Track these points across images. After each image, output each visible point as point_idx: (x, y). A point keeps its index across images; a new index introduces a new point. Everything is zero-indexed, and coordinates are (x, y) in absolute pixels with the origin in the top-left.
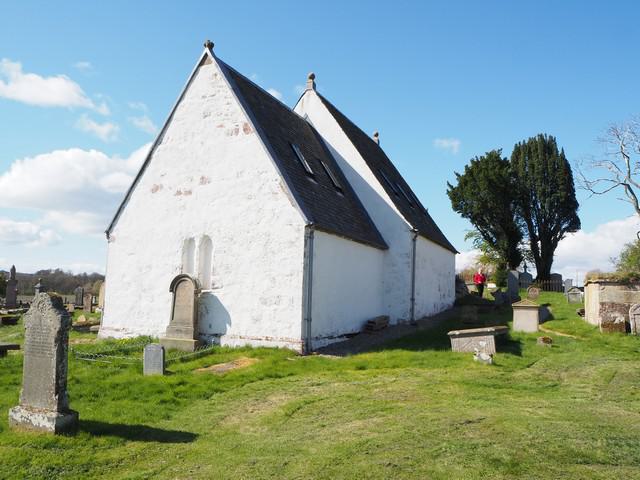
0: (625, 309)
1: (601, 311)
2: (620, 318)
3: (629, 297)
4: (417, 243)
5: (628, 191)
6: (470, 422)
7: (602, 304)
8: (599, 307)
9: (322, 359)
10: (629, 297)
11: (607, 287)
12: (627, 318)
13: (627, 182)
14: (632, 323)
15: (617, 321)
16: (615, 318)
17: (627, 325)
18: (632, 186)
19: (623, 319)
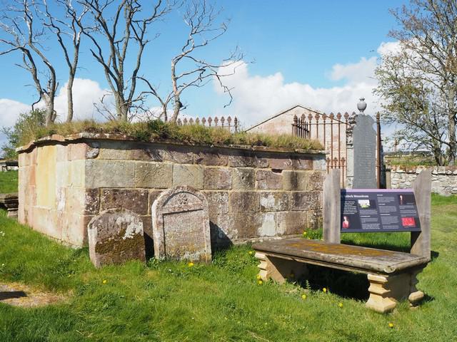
0: (140, 203)
1: (91, 210)
2: (135, 227)
3: (146, 174)
4: (81, 238)
5: (27, 58)
6: (77, 47)
7: (93, 193)
8: (82, 199)
9: (373, 167)
10: (146, 174)
11: (106, 153)
12: (147, 222)
13: (27, 47)
14: (157, 236)
15: (128, 234)
16: (125, 225)
17: (149, 241)
18: (33, 53)
19: (140, 228)
